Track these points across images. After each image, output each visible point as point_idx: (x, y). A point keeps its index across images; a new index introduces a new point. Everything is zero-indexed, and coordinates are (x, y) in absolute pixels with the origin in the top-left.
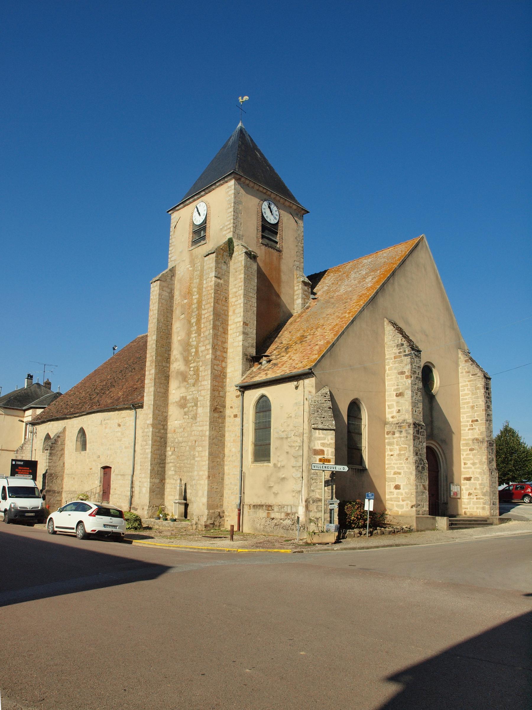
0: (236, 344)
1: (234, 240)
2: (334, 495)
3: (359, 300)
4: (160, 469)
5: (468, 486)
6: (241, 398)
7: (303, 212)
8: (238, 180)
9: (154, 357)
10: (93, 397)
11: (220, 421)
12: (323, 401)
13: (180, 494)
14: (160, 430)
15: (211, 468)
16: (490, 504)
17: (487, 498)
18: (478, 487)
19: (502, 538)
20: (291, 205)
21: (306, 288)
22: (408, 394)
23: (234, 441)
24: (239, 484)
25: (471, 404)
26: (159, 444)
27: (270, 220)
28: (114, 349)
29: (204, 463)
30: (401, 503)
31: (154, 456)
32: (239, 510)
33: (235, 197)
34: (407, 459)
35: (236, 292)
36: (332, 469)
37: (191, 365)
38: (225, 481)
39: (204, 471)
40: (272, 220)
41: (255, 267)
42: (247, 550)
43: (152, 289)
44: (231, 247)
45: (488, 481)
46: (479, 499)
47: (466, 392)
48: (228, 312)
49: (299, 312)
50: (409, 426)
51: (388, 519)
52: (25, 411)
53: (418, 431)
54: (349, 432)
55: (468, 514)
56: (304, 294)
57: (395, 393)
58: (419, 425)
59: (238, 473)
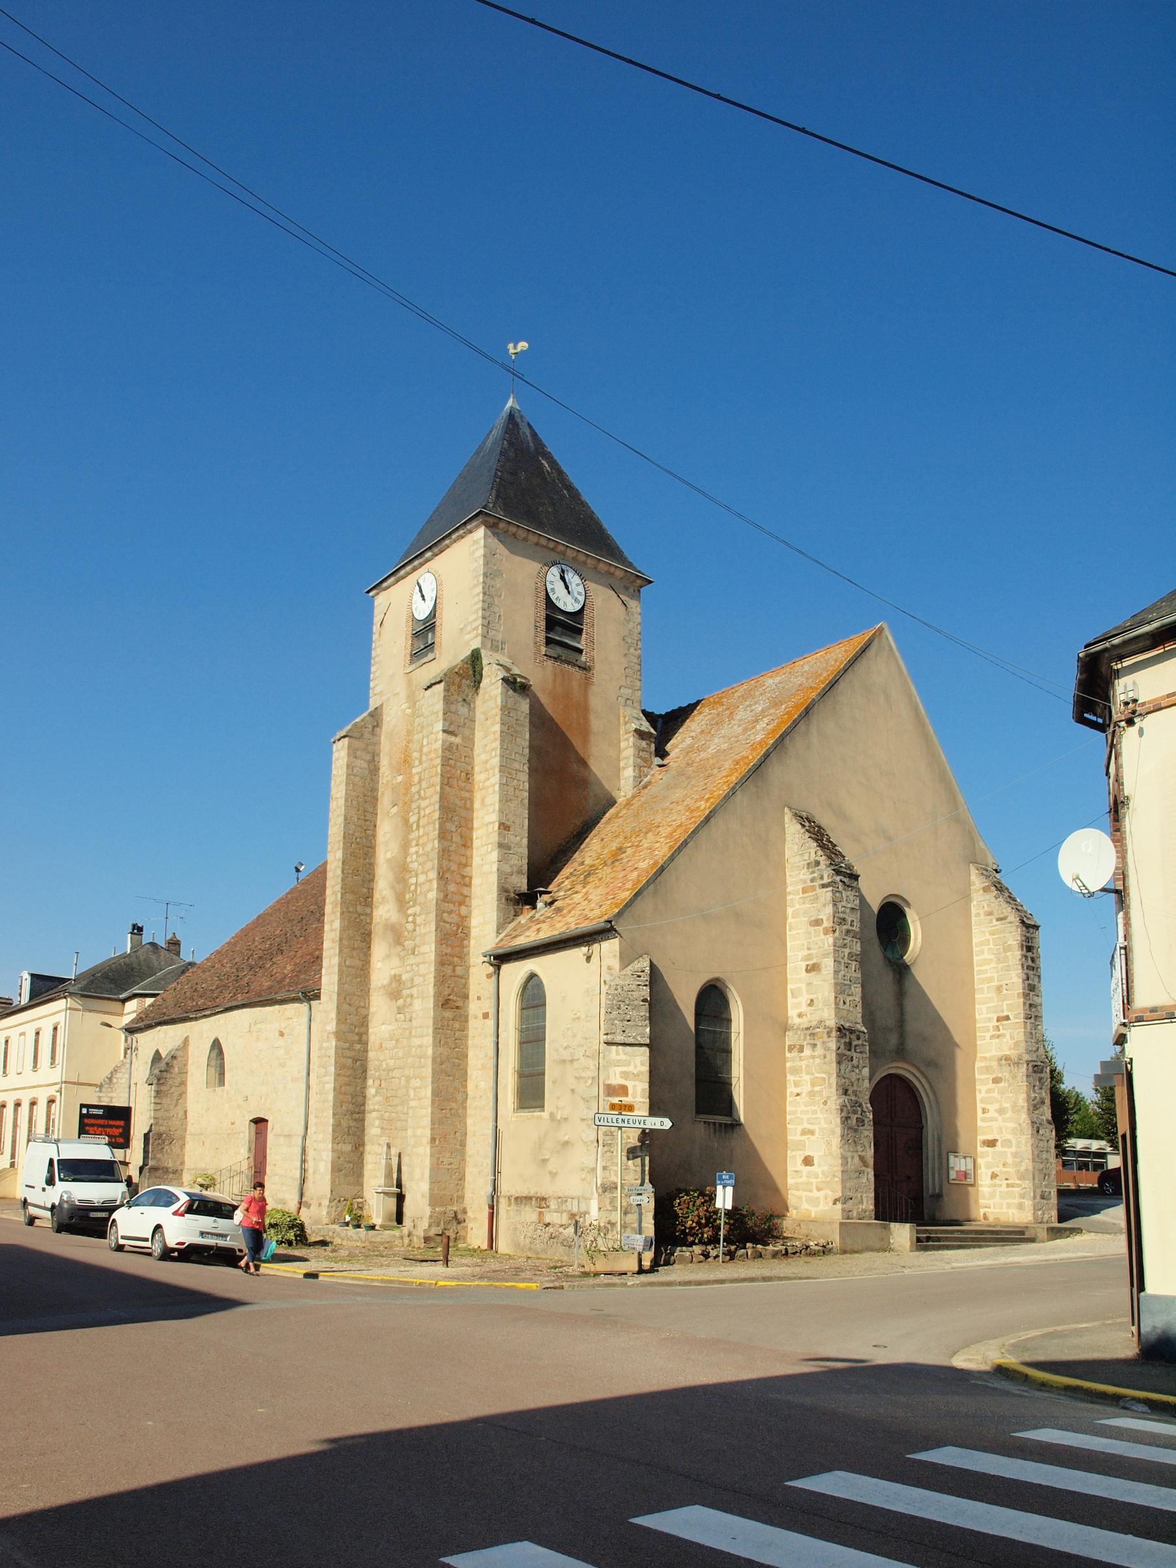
0: (486, 868)
1: (483, 653)
2: (647, 1178)
3: (732, 771)
4: (353, 1124)
5: (989, 1159)
6: (494, 978)
7: (639, 582)
8: (492, 527)
9: (339, 896)
10: (241, 974)
11: (457, 1025)
12: (633, 987)
13: (388, 1175)
14: (352, 1044)
15: (437, 1122)
16: (1034, 1198)
17: (1028, 1184)
18: (1010, 1160)
19: (1020, 1267)
20: (612, 570)
21: (644, 744)
22: (828, 964)
23: (483, 1067)
24: (491, 1154)
25: (996, 983)
26: (350, 1072)
27: (565, 604)
28: (298, 870)
29: (424, 1112)
30: (816, 1194)
31: (341, 1097)
32: (492, 1207)
33: (486, 564)
34: (825, 1103)
35: (487, 762)
36: (642, 1126)
37: (409, 912)
38: (467, 1148)
39: (423, 1127)
40: (568, 604)
41: (525, 706)
42: (453, 1284)
43: (335, 755)
44: (477, 669)
45: (1029, 1148)
46: (1012, 1185)
47: (986, 956)
48: (472, 805)
49: (629, 795)
50: (829, 1034)
51: (788, 1225)
52: (124, 1001)
53: (850, 1043)
54: (699, 1047)
55: (991, 1219)
56: (640, 757)
57: (803, 965)
58: (851, 1031)
59: (490, 1132)
